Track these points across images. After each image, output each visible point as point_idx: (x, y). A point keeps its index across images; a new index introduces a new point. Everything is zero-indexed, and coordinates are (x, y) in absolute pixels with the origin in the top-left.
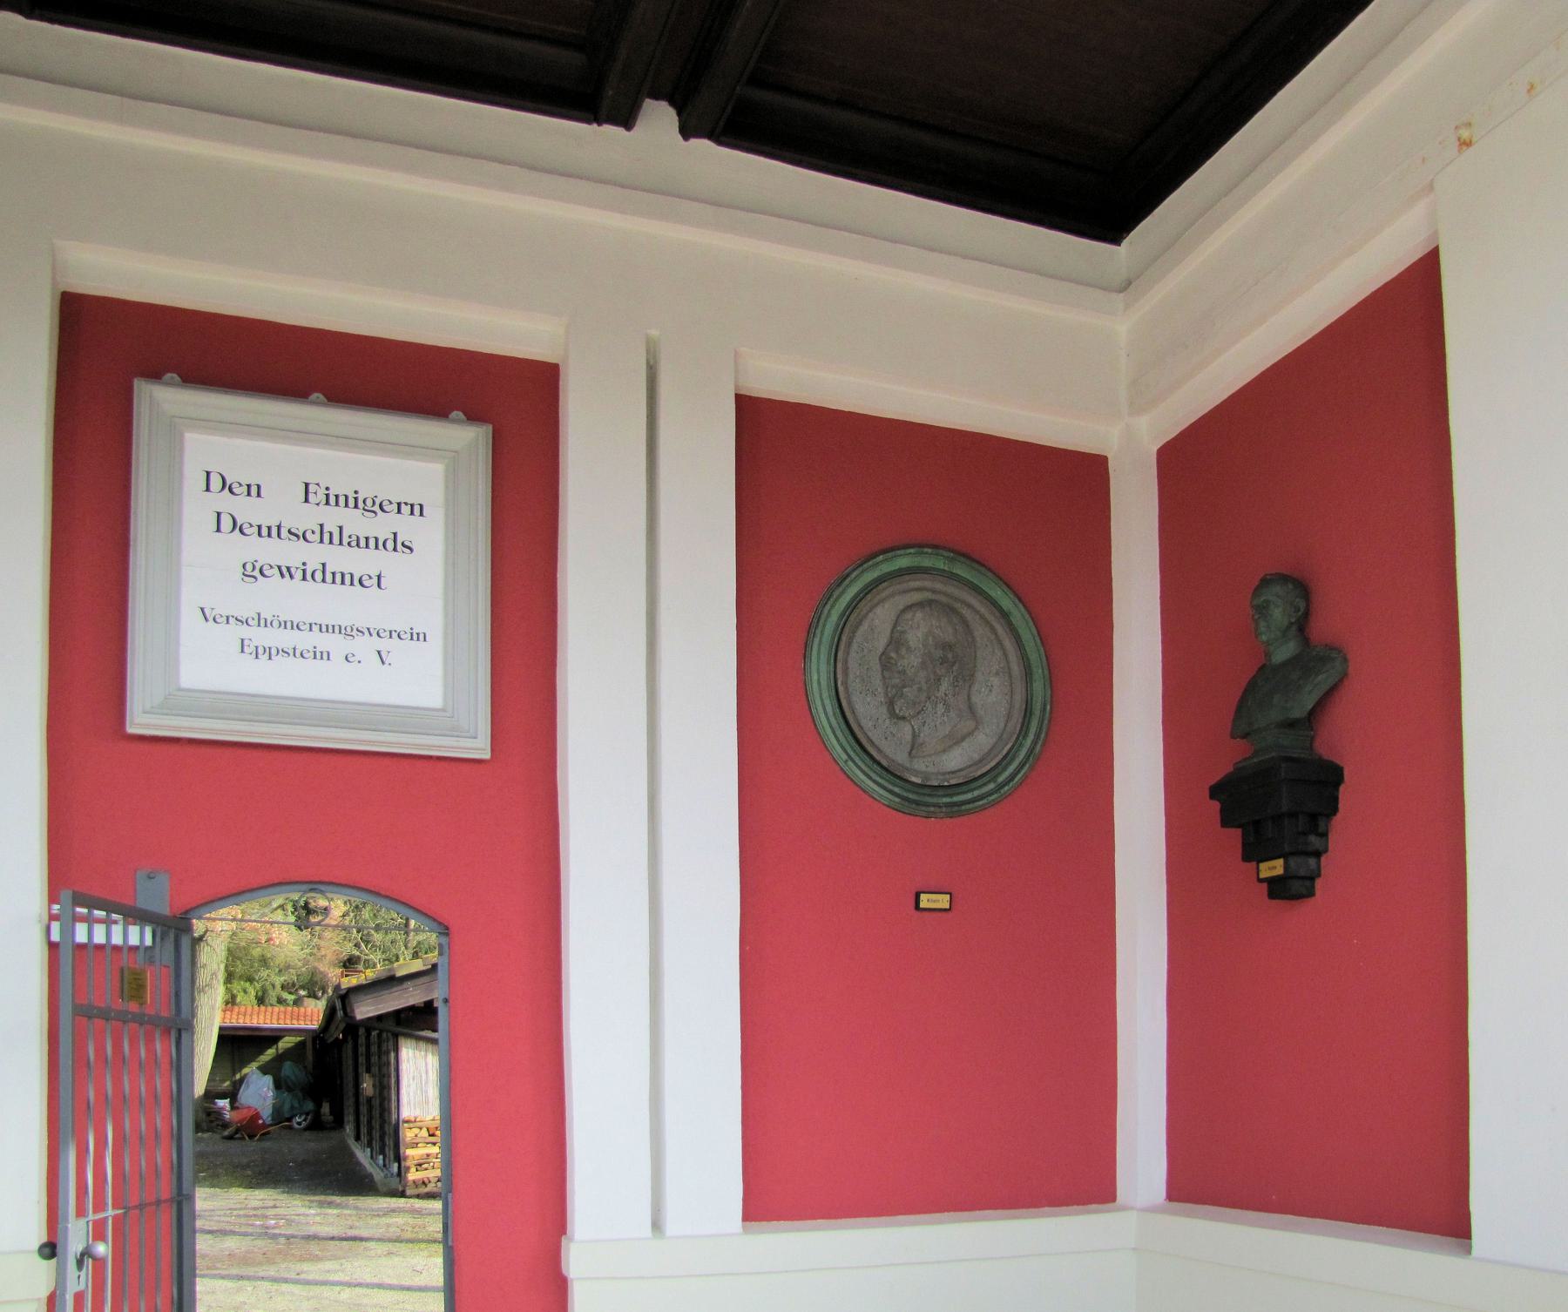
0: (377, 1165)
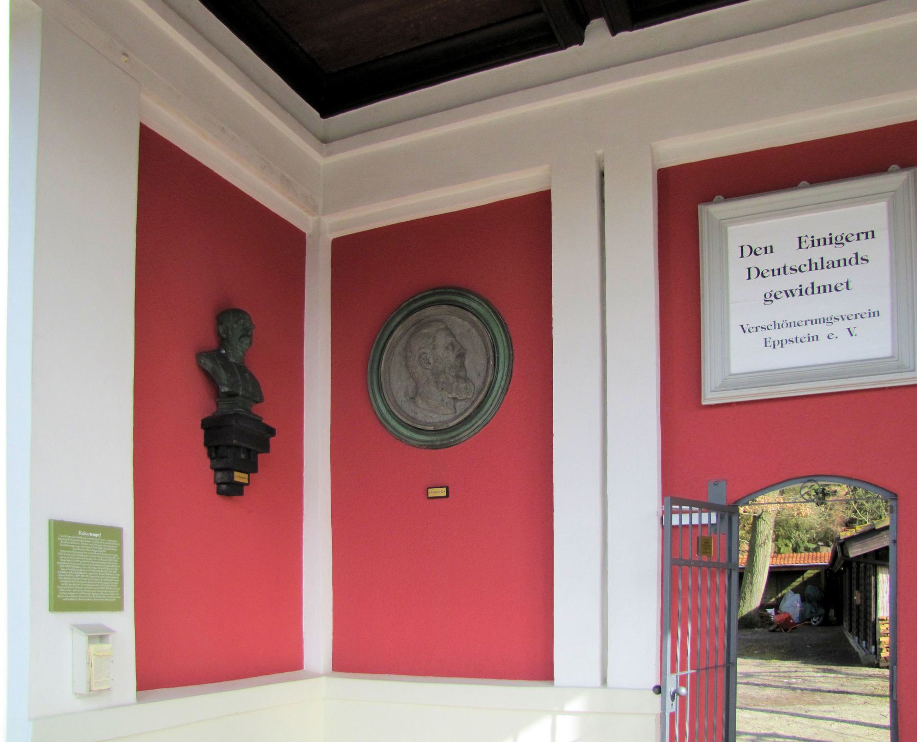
0: (862, 647)
